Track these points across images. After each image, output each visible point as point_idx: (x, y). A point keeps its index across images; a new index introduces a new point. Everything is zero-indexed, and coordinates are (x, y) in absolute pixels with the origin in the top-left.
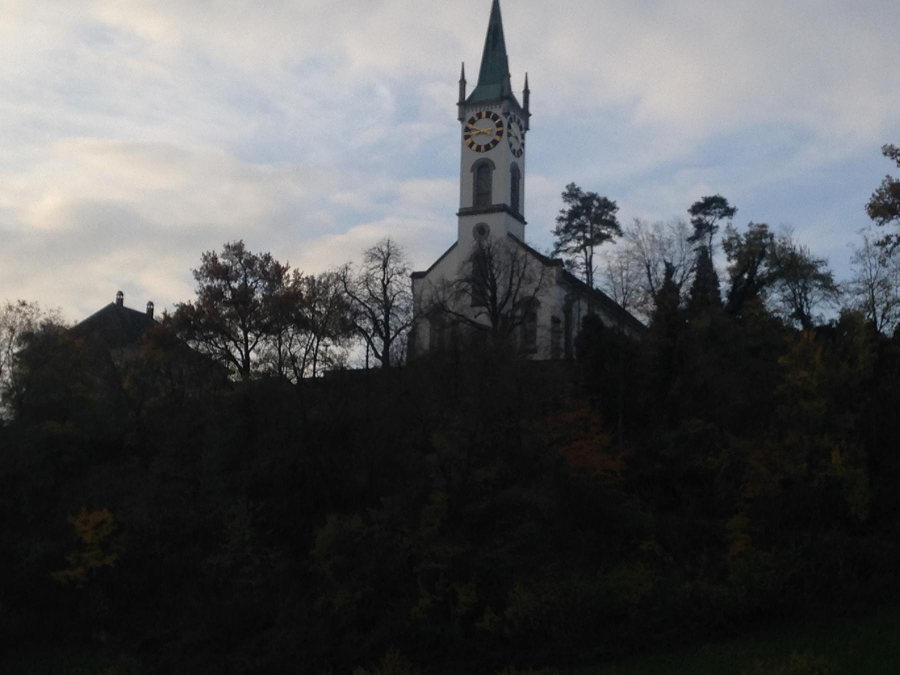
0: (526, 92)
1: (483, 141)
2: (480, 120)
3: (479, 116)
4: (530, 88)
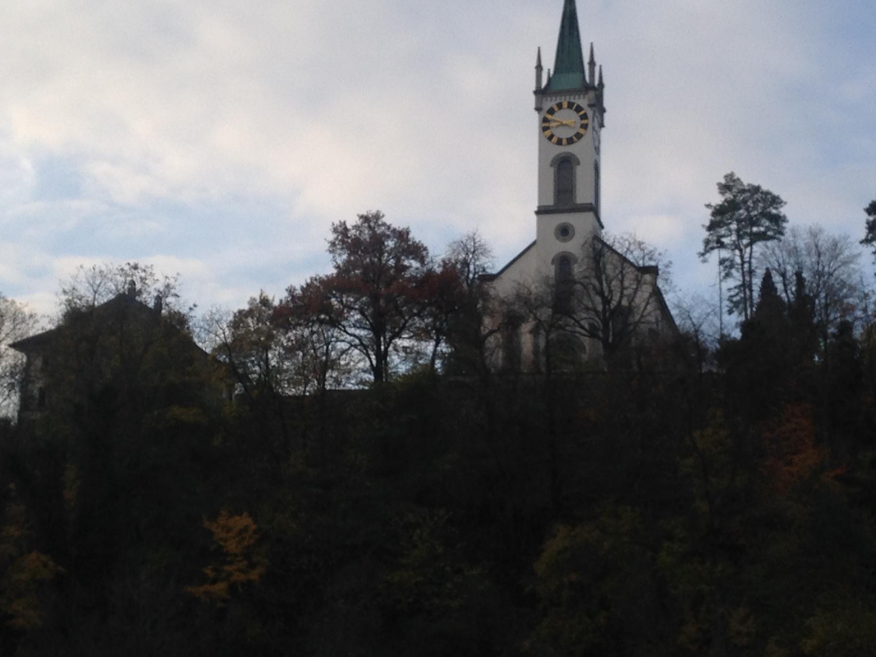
3: (560, 106)
4: (596, 59)
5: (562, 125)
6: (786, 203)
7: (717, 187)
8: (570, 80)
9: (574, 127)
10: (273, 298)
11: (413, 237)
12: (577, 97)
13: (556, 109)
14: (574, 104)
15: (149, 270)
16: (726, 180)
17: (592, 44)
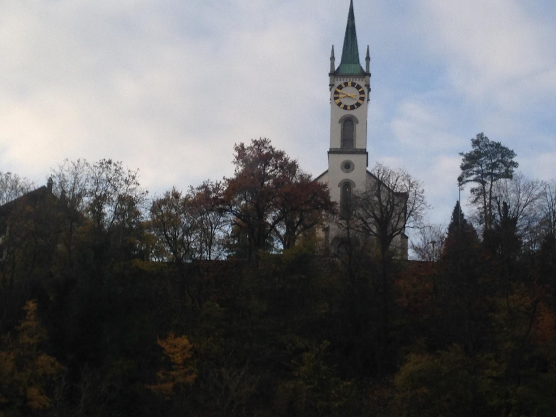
0: (368, 59)
1: (350, 103)
3: (346, 84)
4: (371, 56)
5: (348, 97)
6: (516, 155)
7: (471, 142)
8: (351, 69)
9: (355, 99)
10: (181, 193)
11: (485, 136)
12: (357, 79)
13: (343, 86)
14: (355, 84)
15: (119, 165)
16: (478, 137)
17: (368, 46)
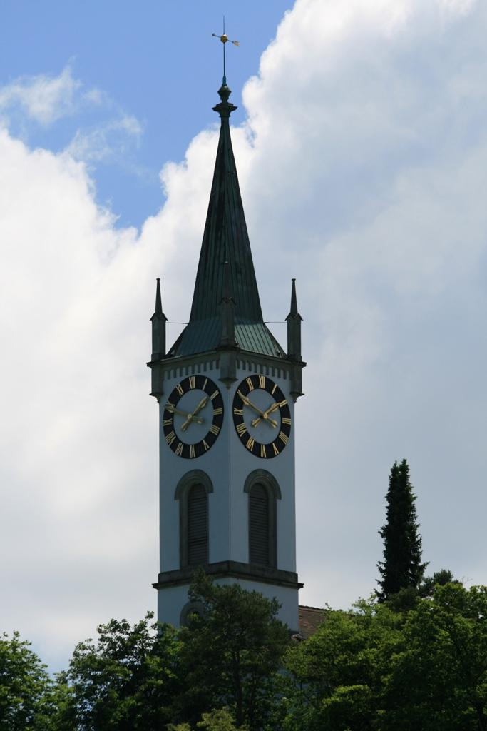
0: (294, 320)
1: (193, 436)
2: (197, 390)
4: (300, 311)
